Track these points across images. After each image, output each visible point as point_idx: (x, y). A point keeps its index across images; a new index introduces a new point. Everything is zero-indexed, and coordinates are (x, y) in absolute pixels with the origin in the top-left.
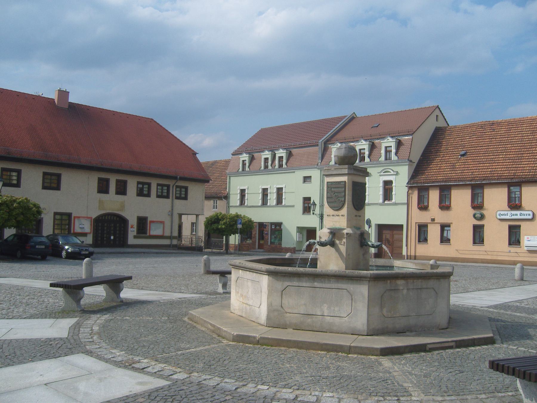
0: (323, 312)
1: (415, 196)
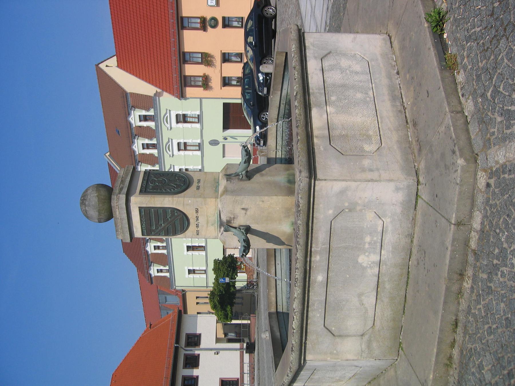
0: (373, 262)
1: (189, 91)
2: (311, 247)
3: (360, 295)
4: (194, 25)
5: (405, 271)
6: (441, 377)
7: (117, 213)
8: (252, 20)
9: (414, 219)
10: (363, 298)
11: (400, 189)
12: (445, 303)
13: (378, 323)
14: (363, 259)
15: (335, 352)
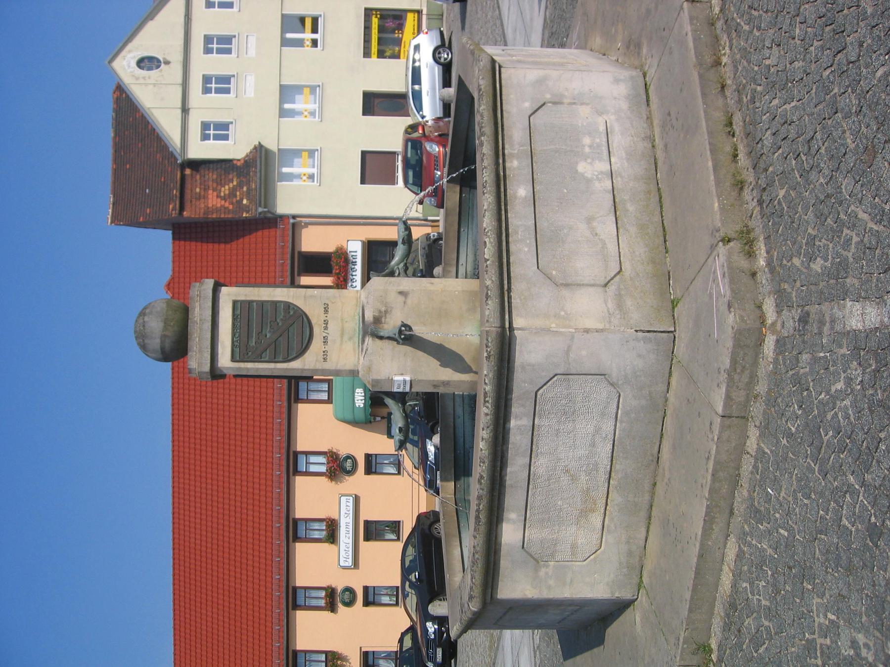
2: (503, 148)
3: (589, 220)
4: (314, 603)
5: (653, 187)
6: (732, 205)
7: (197, 310)
9: (649, 118)
10: (595, 224)
11: (621, 80)
12: (704, 95)
13: (627, 266)
14: (582, 167)
15: (563, 313)
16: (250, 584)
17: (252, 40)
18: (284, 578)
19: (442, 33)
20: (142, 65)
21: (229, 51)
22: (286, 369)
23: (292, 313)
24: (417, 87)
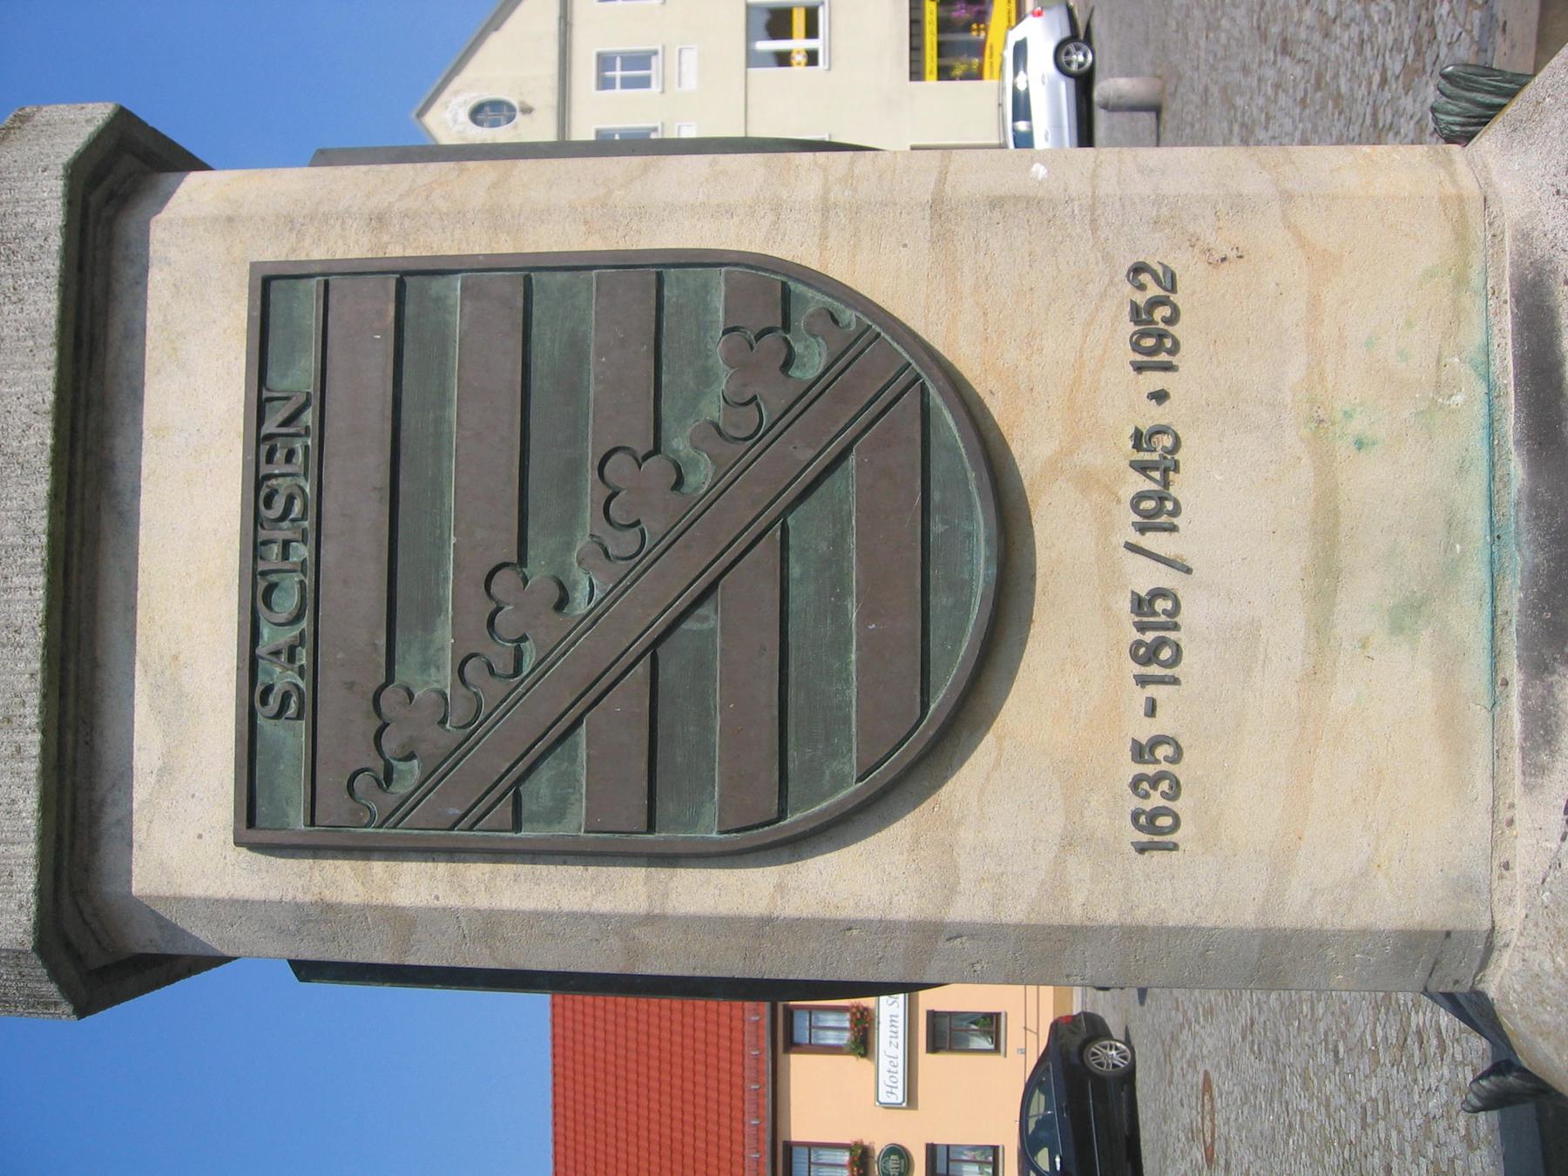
8: (1046, 1092)
16: (701, 1134)
17: (690, 58)
18: (768, 1125)
19: (1070, 12)
20: (479, 117)
21: (645, 83)
22: (765, 927)
23: (813, 360)
24: (1022, 126)
